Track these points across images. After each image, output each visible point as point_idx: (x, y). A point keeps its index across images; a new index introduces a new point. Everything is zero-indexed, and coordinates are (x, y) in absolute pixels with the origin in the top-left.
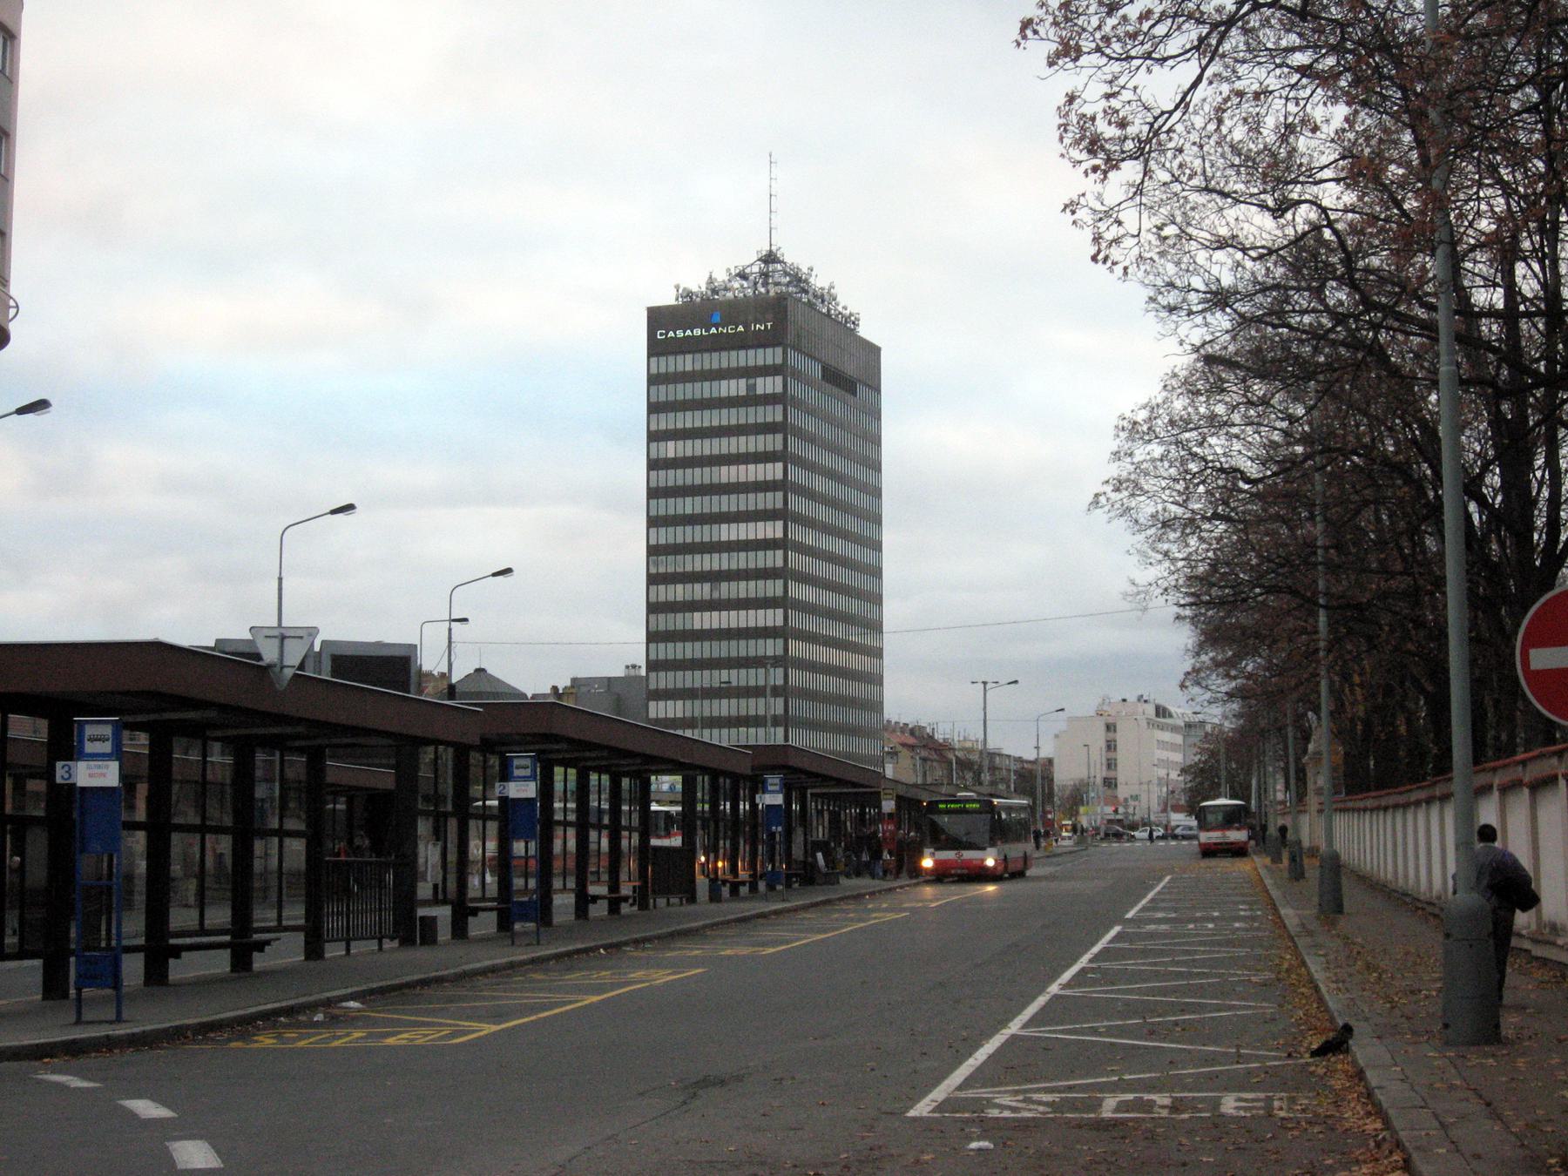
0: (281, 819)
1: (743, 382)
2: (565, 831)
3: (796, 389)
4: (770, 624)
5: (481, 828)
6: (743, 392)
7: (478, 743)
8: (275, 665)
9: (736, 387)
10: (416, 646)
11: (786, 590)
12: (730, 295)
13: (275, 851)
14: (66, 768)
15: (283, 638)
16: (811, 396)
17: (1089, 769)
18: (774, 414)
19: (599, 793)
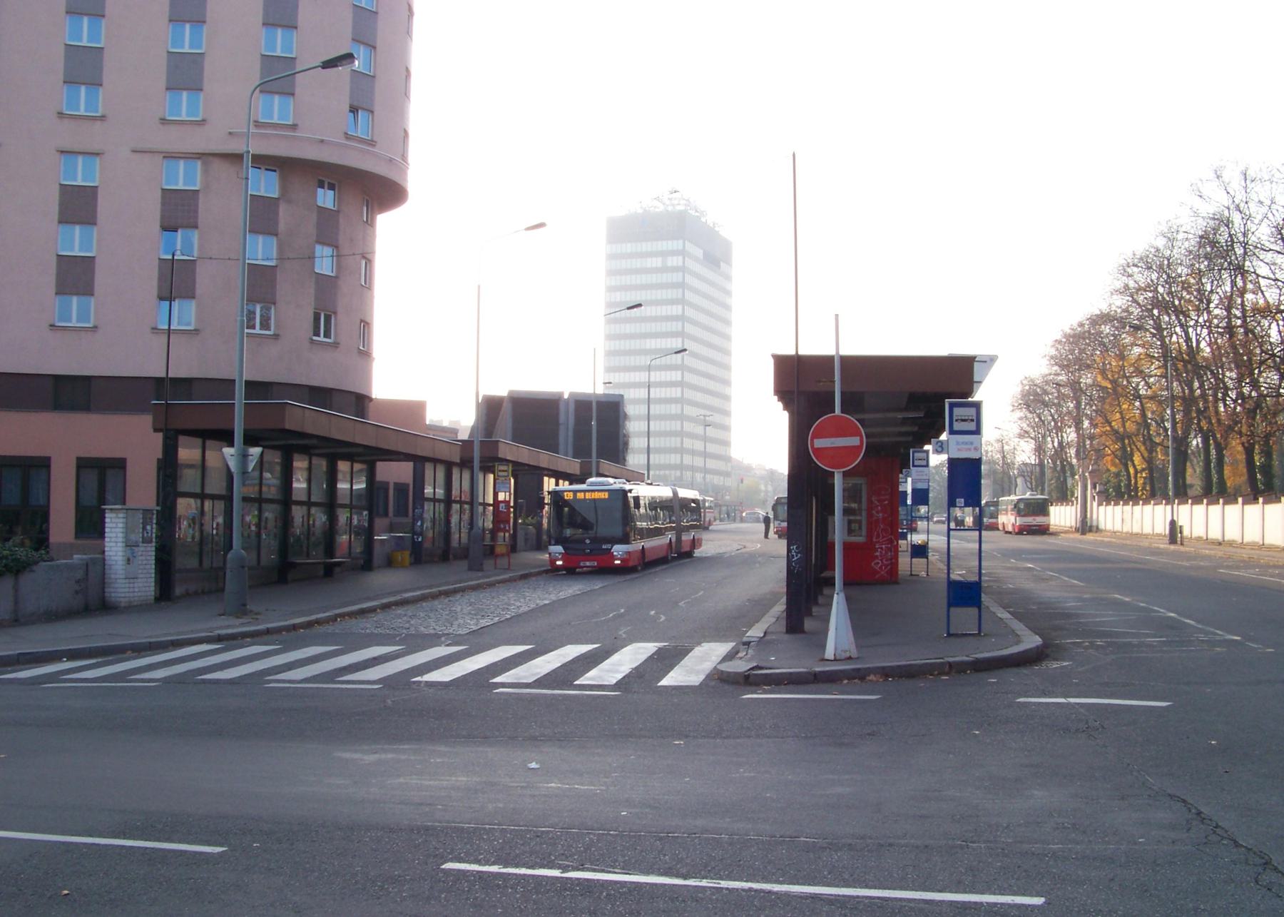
0: (202, 513)
3: (690, 264)
4: (674, 396)
7: (458, 461)
9: (656, 262)
16: (698, 268)
19: (146, 551)
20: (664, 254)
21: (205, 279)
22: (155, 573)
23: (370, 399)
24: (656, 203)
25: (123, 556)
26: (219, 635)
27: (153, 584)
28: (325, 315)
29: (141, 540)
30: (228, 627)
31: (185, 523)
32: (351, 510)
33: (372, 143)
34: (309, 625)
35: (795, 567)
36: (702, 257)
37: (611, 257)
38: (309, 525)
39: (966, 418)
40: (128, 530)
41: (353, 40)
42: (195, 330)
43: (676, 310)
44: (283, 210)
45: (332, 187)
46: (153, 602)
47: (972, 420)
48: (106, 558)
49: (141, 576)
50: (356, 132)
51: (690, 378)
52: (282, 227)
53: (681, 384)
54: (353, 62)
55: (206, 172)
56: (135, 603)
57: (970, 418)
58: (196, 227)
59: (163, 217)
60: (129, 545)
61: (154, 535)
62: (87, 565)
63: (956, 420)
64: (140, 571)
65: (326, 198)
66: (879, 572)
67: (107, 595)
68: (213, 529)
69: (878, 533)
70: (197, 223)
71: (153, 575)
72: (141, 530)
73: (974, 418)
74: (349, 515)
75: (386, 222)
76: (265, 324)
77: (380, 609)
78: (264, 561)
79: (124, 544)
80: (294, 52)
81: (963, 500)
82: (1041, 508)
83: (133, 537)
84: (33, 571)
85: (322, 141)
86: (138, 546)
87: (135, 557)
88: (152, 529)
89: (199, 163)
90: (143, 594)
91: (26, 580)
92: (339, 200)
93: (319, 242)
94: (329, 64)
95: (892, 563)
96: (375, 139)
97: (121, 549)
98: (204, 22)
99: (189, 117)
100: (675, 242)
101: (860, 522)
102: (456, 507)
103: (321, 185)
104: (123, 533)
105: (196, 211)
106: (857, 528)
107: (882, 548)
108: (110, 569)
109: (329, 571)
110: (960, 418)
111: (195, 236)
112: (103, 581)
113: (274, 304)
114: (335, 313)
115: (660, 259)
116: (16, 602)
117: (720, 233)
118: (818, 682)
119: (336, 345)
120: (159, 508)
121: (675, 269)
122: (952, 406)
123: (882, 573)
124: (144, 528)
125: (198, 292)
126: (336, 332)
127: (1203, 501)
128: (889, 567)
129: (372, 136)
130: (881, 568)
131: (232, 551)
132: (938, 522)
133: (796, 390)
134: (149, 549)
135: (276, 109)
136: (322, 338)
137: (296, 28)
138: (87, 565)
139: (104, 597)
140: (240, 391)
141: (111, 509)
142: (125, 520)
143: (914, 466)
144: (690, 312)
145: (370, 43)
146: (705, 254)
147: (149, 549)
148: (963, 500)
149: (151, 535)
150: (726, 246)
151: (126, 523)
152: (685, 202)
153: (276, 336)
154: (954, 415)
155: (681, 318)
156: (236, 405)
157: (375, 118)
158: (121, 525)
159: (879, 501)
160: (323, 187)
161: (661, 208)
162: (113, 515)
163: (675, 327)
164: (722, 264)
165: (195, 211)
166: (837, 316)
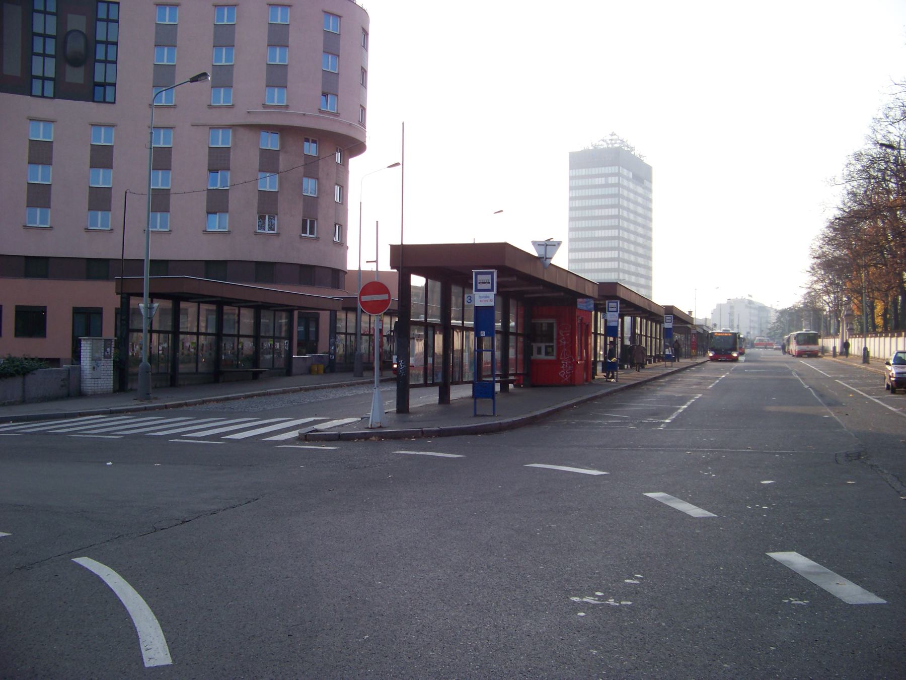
1: (603, 179)
2: (274, 334)
3: (623, 181)
5: (667, 379)
6: (603, 183)
8: (543, 258)
9: (601, 181)
10: (101, 336)
11: (619, 265)
12: (602, 147)
13: (203, 324)
14: (469, 298)
15: (547, 245)
16: (629, 184)
17: (346, 342)
18: (614, 190)
20: (606, 176)
21: (234, 201)
22: (113, 375)
23: (345, 272)
24: (602, 143)
25: (90, 366)
26: (111, 410)
27: (112, 382)
28: (310, 220)
29: (103, 356)
30: (127, 406)
31: (137, 347)
32: (274, 340)
33: (337, 115)
34: (180, 405)
35: (402, 373)
36: (631, 177)
37: (572, 178)
38: (238, 348)
39: (485, 281)
40: (93, 351)
41: (324, 52)
42: (229, 231)
43: (614, 212)
44: (282, 157)
45: (314, 142)
46: (112, 392)
47: (489, 283)
48: (82, 367)
49: (103, 377)
50: (327, 108)
51: (624, 255)
52: (281, 167)
53: (618, 259)
54: (207, 78)
55: (234, 135)
56: (99, 393)
57: (488, 281)
58: (229, 169)
59: (209, 164)
60: (94, 359)
61: (112, 354)
62: (69, 370)
63: (479, 283)
64: (102, 374)
65: (311, 149)
66: (564, 379)
67: (82, 388)
68: (159, 350)
69: (563, 354)
70: (229, 167)
71: (112, 377)
72: (103, 351)
73: (490, 281)
74: (272, 343)
75: (355, 164)
76: (271, 228)
77: (243, 398)
78: (201, 369)
79: (91, 359)
80: (287, 61)
81: (484, 332)
82: (812, 339)
83: (97, 355)
84: (34, 374)
85: (304, 115)
86: (101, 360)
87: (98, 366)
88: (112, 351)
89: (231, 131)
90: (105, 387)
91: (30, 378)
92: (319, 150)
93: (305, 176)
94: (194, 80)
95: (571, 374)
96: (339, 112)
97: (88, 362)
98: (234, 46)
99: (225, 103)
100: (613, 168)
101: (552, 346)
102: (512, 338)
103: (307, 140)
104: (90, 352)
105: (229, 160)
106: (551, 351)
107: (565, 364)
108: (83, 373)
109: (256, 376)
110: (481, 281)
111: (228, 174)
112: (80, 380)
113: (277, 215)
114: (317, 219)
115: (603, 179)
116: (24, 391)
117: (644, 161)
118: (341, 440)
119: (317, 239)
120: (116, 338)
121: (612, 185)
122: (477, 274)
123: (566, 379)
124: (105, 350)
125: (230, 209)
126: (317, 231)
127: (902, 334)
128: (570, 376)
129: (337, 110)
130: (565, 376)
131: (142, 363)
132: (776, 349)
133: (401, 266)
134: (109, 362)
135: (277, 97)
136: (308, 235)
137: (288, 46)
138: (69, 370)
139: (80, 389)
140: (147, 267)
141: (84, 339)
142: (91, 345)
143: (608, 311)
144: (623, 213)
145: (336, 53)
146: (634, 175)
147: (109, 362)
148: (484, 332)
149: (111, 353)
150: (649, 169)
151: (92, 347)
152: (619, 141)
153: (278, 234)
154: (478, 279)
155: (618, 217)
156: (145, 279)
157: (339, 100)
158: (88, 348)
159: (564, 334)
160: (309, 142)
161: (605, 146)
162: (85, 342)
163: (614, 222)
164: (645, 181)
165: (228, 160)
166: (377, 222)
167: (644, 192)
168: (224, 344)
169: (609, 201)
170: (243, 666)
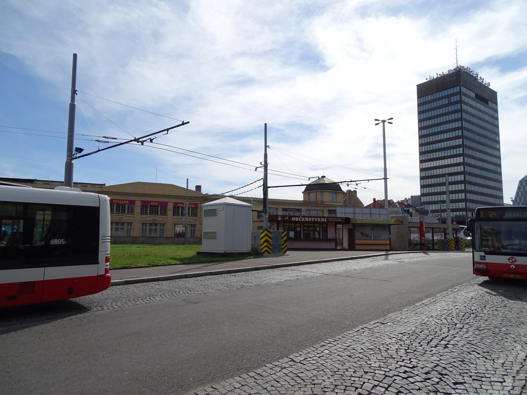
1: (447, 100)
9: (446, 101)
20: (449, 96)
121: (455, 103)
167: (491, 112)
168: (49, 184)
169: (453, 117)
170: (480, 326)
